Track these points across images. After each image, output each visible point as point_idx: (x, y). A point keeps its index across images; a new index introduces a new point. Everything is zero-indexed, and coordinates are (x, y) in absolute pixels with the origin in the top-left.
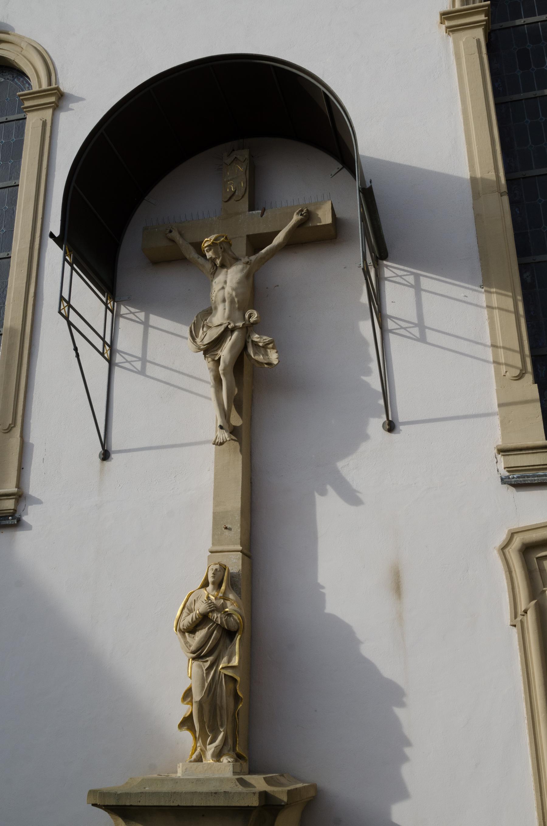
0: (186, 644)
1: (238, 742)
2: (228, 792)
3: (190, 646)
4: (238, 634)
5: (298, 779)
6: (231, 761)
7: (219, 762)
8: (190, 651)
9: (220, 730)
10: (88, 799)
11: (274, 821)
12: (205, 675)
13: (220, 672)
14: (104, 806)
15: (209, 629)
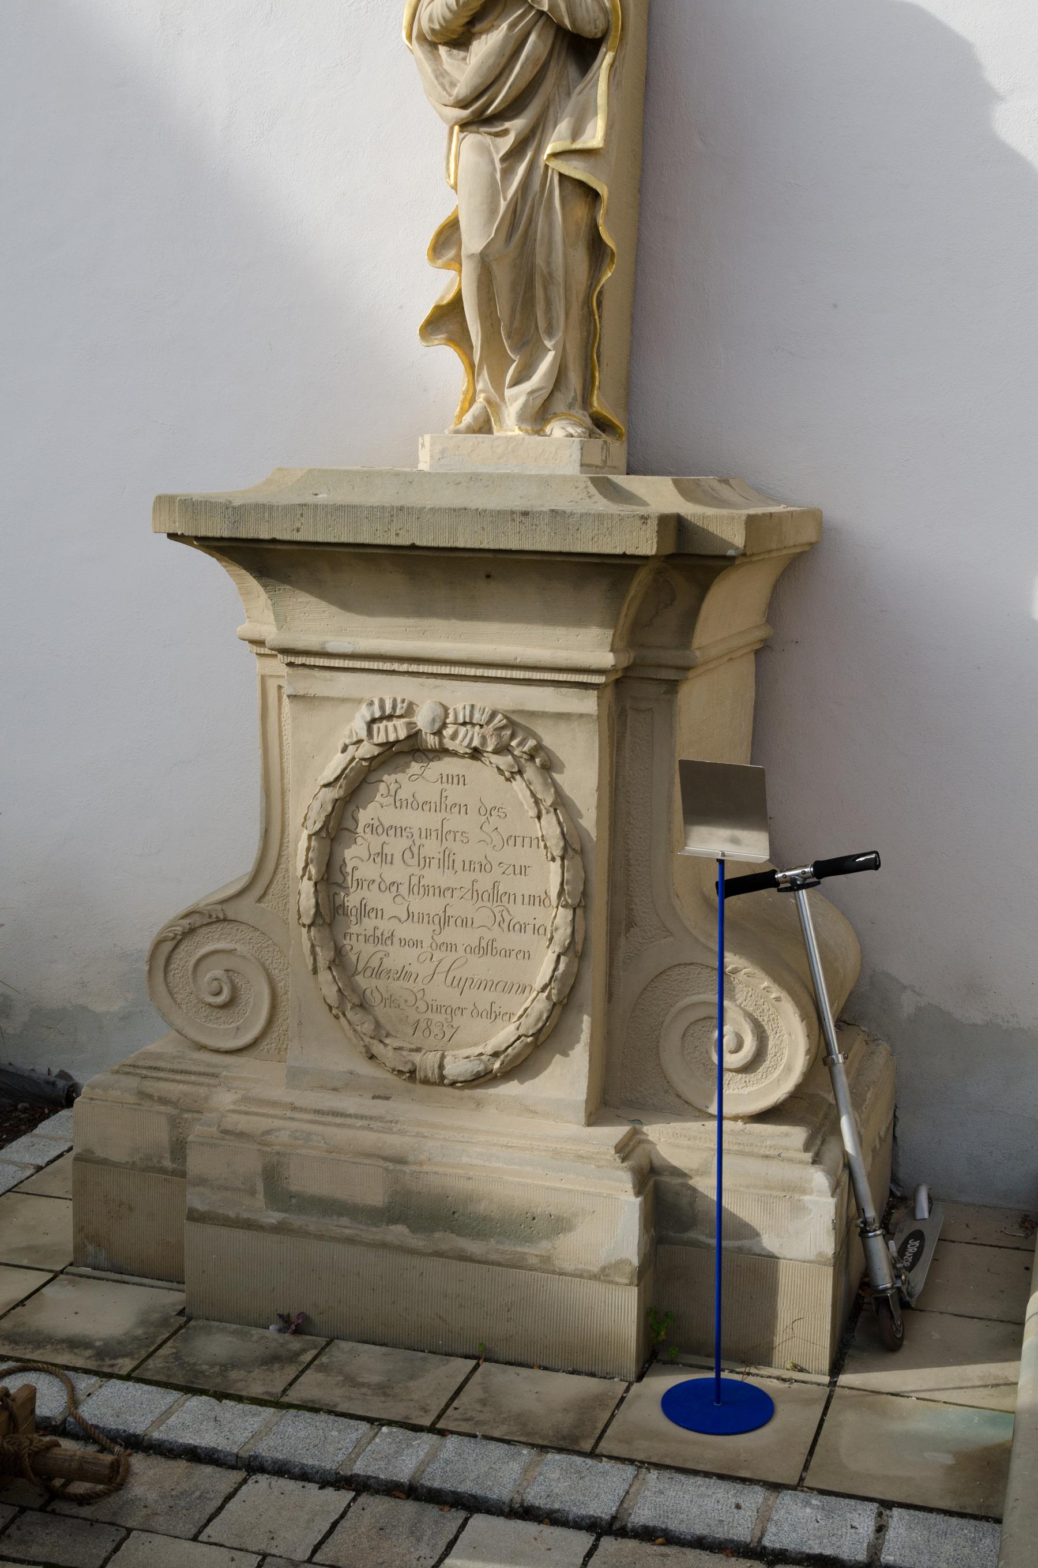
0: (441, 78)
1: (597, 383)
2: (565, 512)
3: (453, 84)
4: (604, 50)
5: (769, 497)
6: (575, 434)
7: (539, 435)
8: (452, 98)
9: (546, 346)
10: (154, 519)
11: (701, 599)
12: (498, 176)
13: (547, 167)
14: (197, 538)
15: (512, 26)
